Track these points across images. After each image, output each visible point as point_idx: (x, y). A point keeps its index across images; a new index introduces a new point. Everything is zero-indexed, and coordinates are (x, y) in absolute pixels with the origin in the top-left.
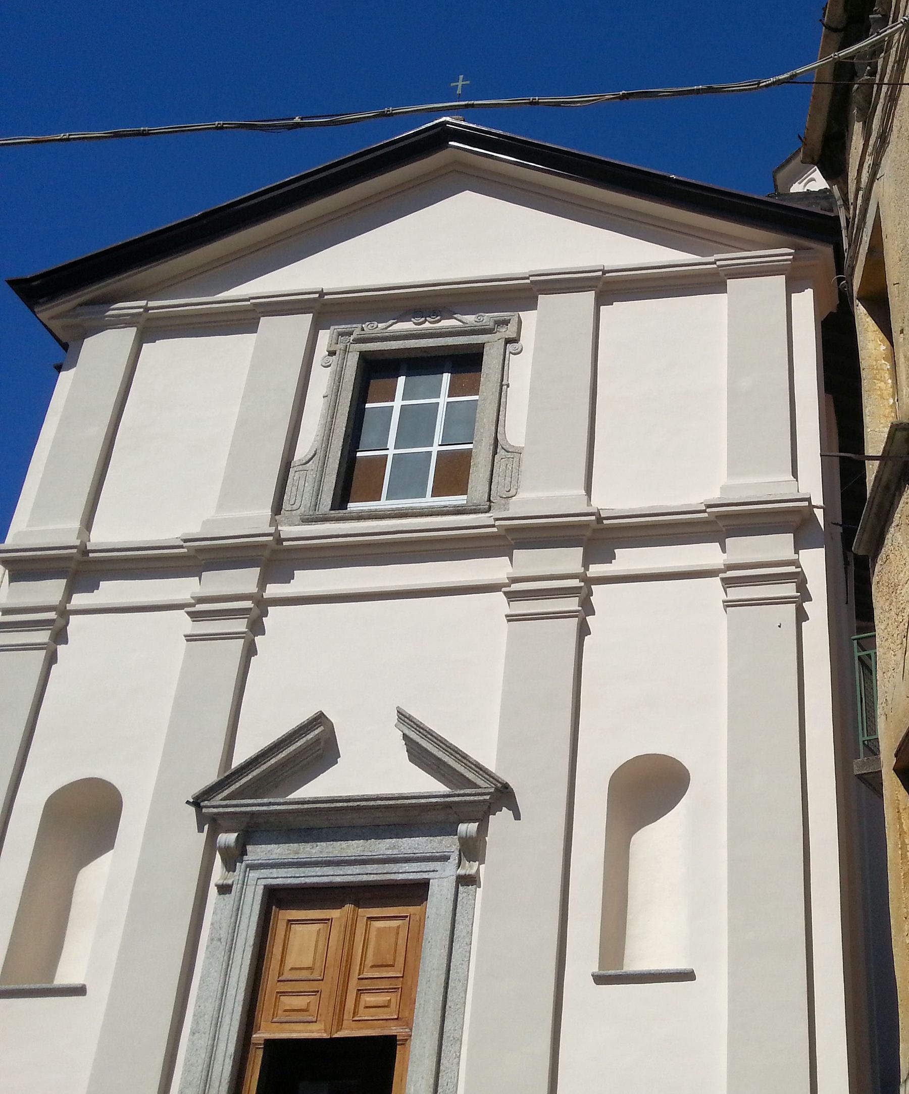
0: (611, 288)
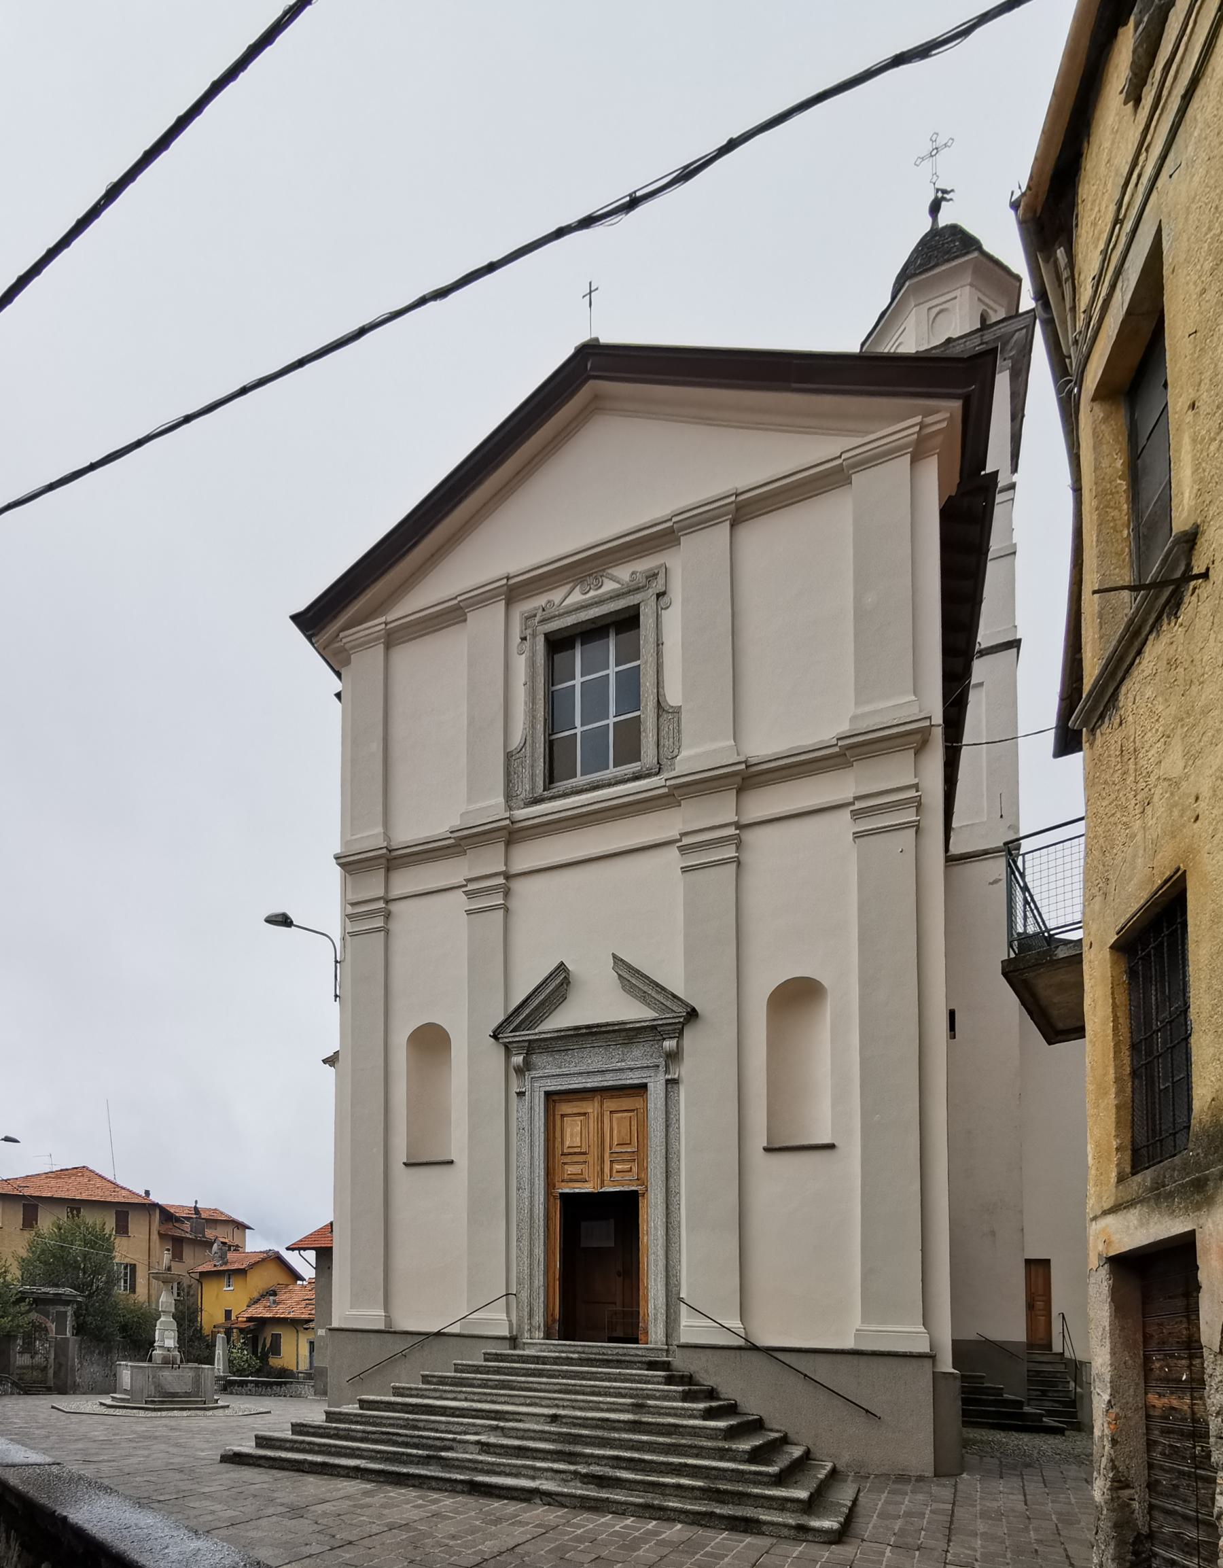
0: (742, 511)
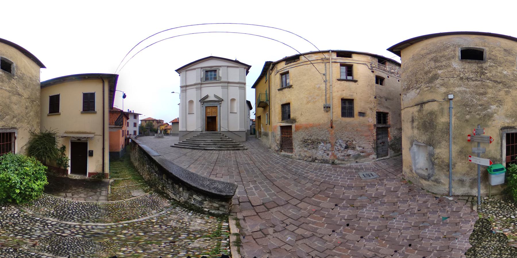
0: (228, 67)
